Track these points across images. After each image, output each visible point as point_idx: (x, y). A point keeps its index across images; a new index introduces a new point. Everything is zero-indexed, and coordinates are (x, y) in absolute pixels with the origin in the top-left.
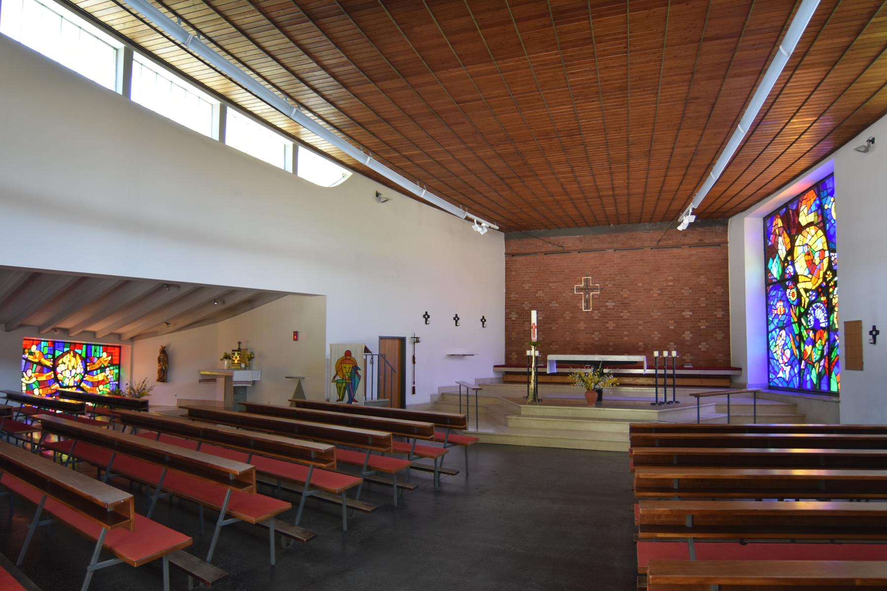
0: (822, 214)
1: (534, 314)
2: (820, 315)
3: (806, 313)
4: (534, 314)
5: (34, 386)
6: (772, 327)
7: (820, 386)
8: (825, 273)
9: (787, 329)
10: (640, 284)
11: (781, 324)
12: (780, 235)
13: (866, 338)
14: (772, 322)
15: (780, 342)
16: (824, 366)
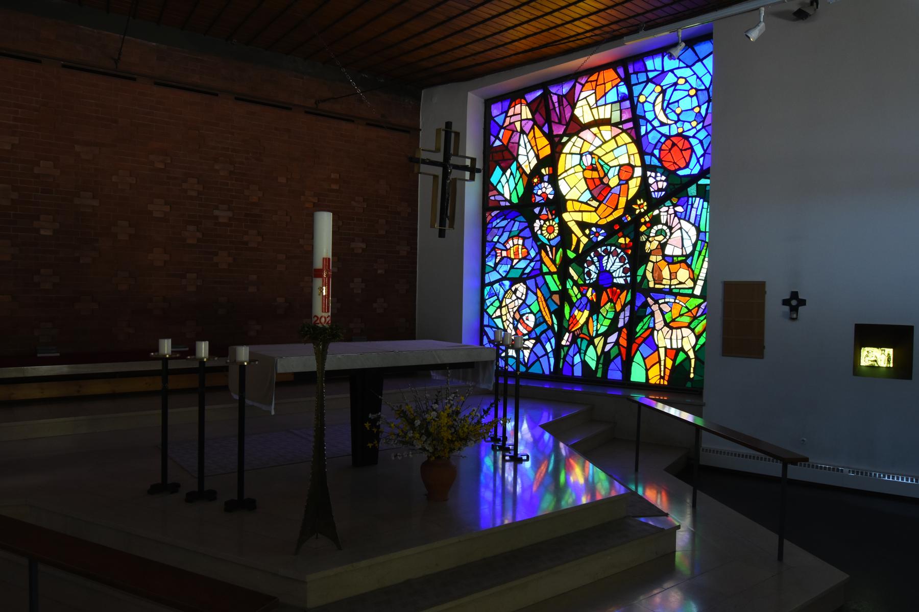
0: (633, 108)
1: (325, 223)
2: (615, 266)
3: (581, 260)
4: (325, 223)
5: (546, 178)
6: (493, 276)
7: (605, 372)
8: (630, 203)
9: (531, 283)
10: (282, 180)
11: (515, 274)
12: (522, 132)
13: (774, 307)
14: (495, 269)
15: (512, 303)
16: (617, 343)
